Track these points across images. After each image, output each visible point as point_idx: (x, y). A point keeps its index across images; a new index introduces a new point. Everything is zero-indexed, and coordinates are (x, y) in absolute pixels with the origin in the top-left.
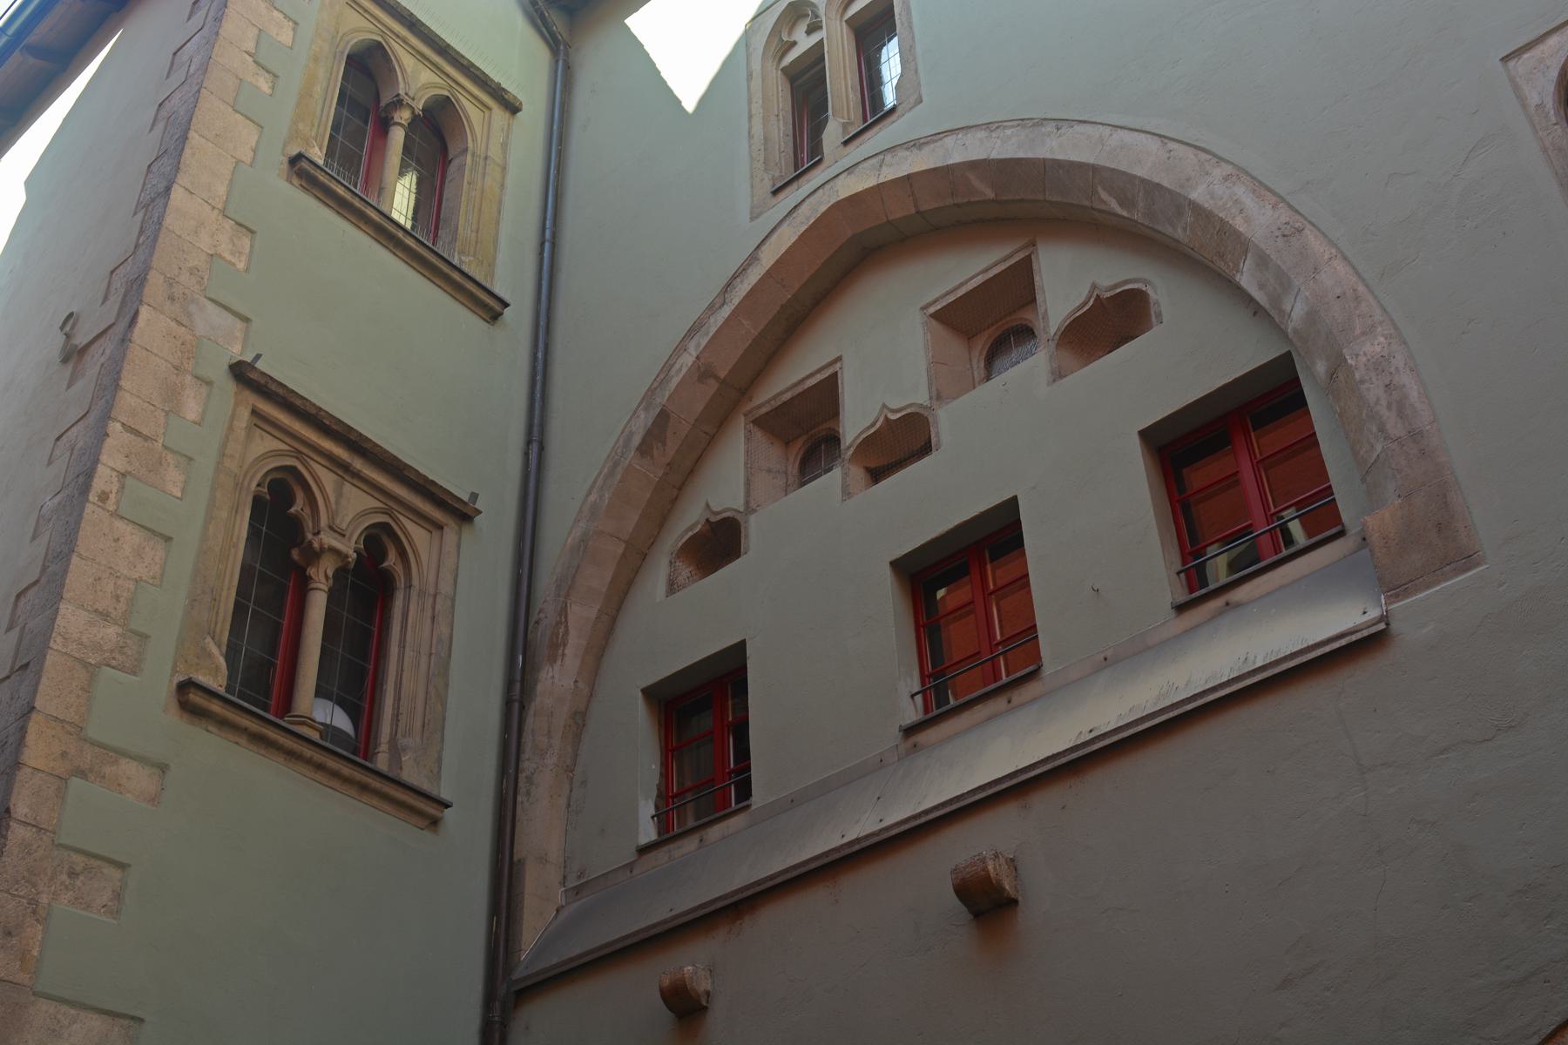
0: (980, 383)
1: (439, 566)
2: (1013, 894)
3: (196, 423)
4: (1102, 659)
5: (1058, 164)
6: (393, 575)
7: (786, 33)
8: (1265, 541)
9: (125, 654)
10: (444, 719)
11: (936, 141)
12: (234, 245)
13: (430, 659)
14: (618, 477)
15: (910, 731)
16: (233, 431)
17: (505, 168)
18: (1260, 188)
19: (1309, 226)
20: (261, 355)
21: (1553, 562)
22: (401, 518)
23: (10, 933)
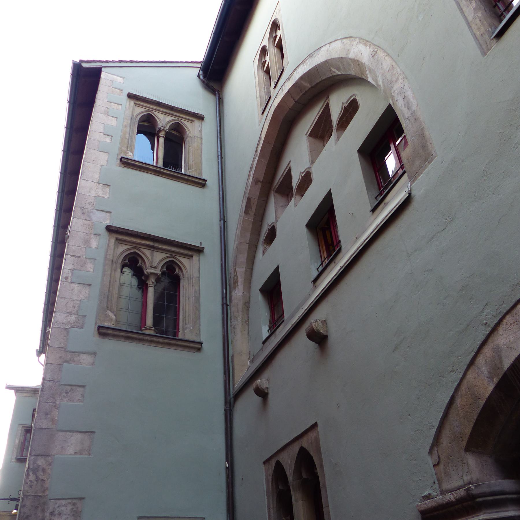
3: (96, 248)
10: (200, 316)
12: (103, 191)
16: (109, 247)
18: (365, 42)
21: (457, 145)
22: (177, 257)
23: (47, 414)
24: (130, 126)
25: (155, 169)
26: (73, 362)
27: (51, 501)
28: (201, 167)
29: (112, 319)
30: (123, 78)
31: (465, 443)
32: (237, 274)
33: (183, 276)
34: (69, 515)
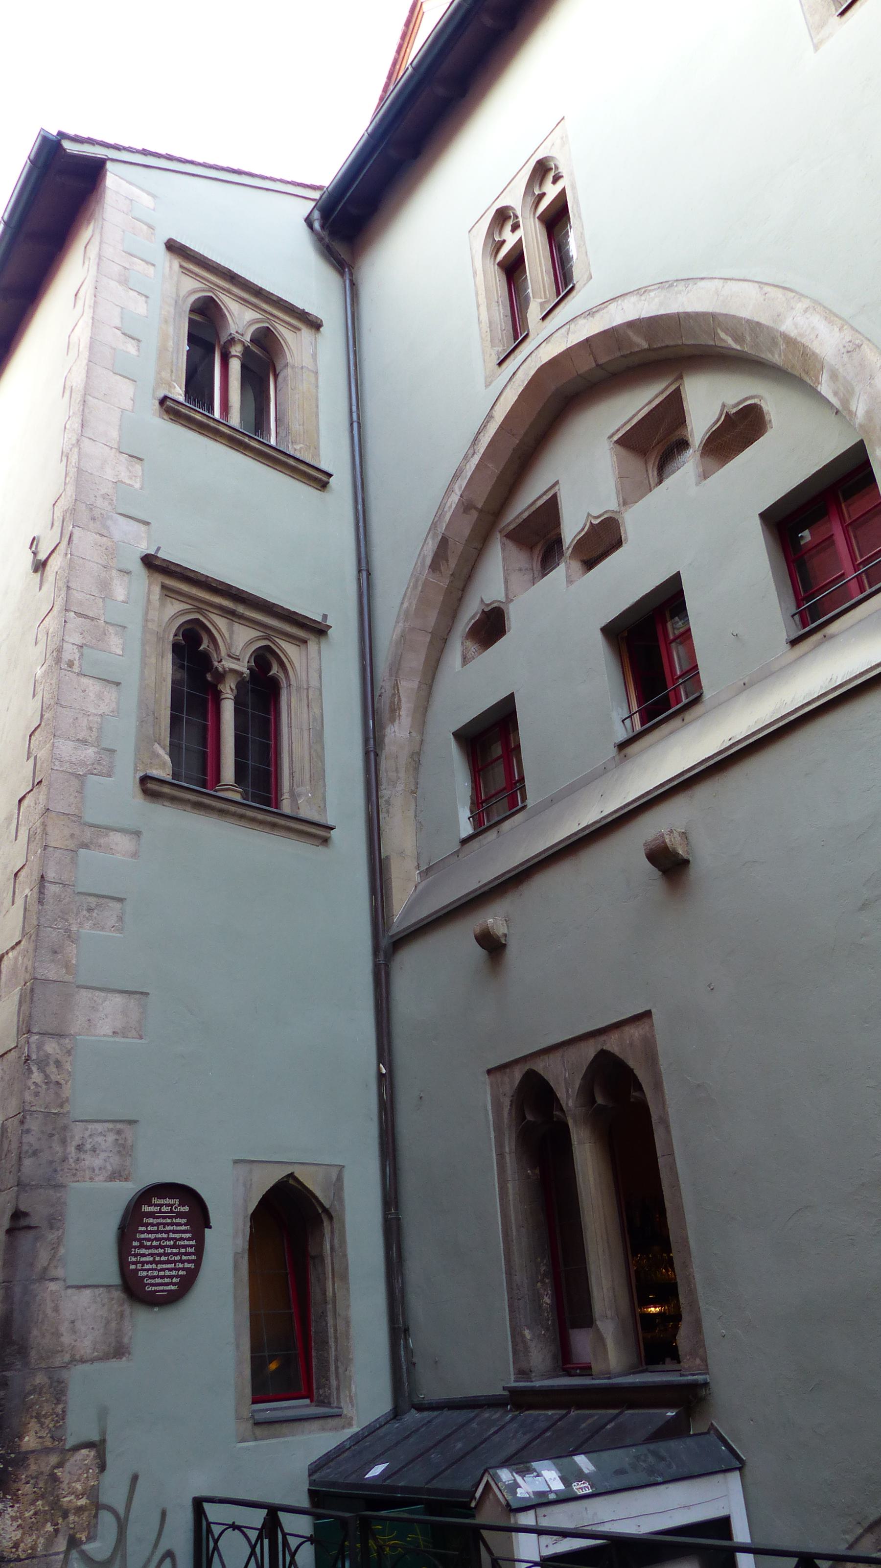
0: (654, 487)
1: (308, 669)
2: (685, 856)
3: (125, 603)
4: (743, 685)
5: (687, 315)
6: (278, 680)
7: (498, 235)
8: (854, 585)
9: (101, 764)
11: (603, 309)
12: (130, 472)
13: (310, 732)
14: (420, 588)
15: (623, 746)
17: (317, 373)
18: (830, 315)
19: (866, 342)
20: (160, 547)
22: (277, 640)
24: (174, 319)
25: (232, 433)
26: (97, 848)
27: (76, 1125)
28: (319, 443)
29: (164, 763)
30: (154, 196)
32: (398, 692)
33: (287, 683)
34: (111, 1151)
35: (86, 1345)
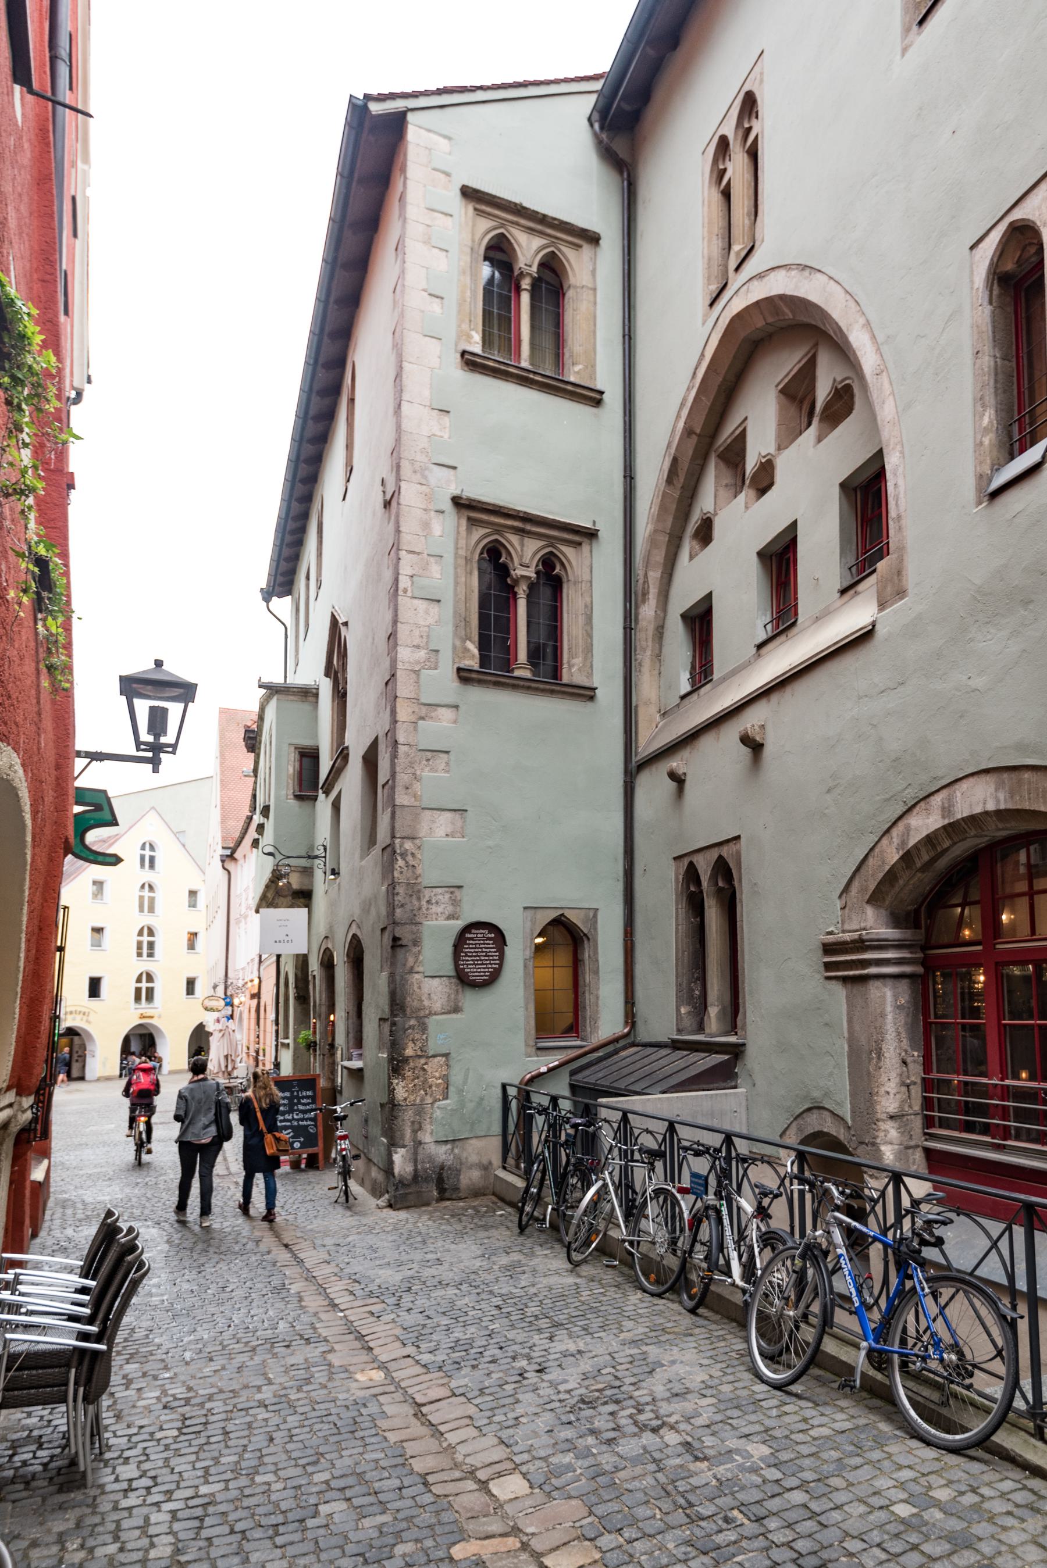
2: (761, 741)
15: (760, 646)
28: (595, 359)
29: (473, 656)
31: (867, 897)
35: (437, 1006)
